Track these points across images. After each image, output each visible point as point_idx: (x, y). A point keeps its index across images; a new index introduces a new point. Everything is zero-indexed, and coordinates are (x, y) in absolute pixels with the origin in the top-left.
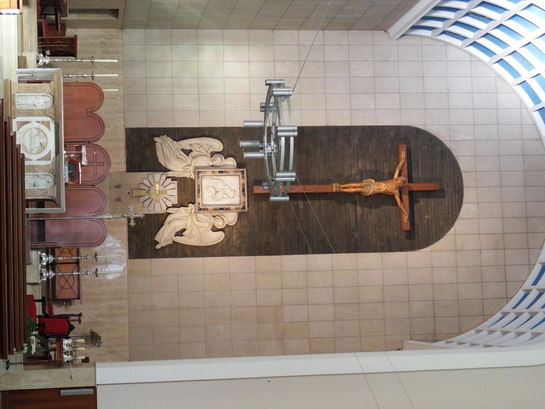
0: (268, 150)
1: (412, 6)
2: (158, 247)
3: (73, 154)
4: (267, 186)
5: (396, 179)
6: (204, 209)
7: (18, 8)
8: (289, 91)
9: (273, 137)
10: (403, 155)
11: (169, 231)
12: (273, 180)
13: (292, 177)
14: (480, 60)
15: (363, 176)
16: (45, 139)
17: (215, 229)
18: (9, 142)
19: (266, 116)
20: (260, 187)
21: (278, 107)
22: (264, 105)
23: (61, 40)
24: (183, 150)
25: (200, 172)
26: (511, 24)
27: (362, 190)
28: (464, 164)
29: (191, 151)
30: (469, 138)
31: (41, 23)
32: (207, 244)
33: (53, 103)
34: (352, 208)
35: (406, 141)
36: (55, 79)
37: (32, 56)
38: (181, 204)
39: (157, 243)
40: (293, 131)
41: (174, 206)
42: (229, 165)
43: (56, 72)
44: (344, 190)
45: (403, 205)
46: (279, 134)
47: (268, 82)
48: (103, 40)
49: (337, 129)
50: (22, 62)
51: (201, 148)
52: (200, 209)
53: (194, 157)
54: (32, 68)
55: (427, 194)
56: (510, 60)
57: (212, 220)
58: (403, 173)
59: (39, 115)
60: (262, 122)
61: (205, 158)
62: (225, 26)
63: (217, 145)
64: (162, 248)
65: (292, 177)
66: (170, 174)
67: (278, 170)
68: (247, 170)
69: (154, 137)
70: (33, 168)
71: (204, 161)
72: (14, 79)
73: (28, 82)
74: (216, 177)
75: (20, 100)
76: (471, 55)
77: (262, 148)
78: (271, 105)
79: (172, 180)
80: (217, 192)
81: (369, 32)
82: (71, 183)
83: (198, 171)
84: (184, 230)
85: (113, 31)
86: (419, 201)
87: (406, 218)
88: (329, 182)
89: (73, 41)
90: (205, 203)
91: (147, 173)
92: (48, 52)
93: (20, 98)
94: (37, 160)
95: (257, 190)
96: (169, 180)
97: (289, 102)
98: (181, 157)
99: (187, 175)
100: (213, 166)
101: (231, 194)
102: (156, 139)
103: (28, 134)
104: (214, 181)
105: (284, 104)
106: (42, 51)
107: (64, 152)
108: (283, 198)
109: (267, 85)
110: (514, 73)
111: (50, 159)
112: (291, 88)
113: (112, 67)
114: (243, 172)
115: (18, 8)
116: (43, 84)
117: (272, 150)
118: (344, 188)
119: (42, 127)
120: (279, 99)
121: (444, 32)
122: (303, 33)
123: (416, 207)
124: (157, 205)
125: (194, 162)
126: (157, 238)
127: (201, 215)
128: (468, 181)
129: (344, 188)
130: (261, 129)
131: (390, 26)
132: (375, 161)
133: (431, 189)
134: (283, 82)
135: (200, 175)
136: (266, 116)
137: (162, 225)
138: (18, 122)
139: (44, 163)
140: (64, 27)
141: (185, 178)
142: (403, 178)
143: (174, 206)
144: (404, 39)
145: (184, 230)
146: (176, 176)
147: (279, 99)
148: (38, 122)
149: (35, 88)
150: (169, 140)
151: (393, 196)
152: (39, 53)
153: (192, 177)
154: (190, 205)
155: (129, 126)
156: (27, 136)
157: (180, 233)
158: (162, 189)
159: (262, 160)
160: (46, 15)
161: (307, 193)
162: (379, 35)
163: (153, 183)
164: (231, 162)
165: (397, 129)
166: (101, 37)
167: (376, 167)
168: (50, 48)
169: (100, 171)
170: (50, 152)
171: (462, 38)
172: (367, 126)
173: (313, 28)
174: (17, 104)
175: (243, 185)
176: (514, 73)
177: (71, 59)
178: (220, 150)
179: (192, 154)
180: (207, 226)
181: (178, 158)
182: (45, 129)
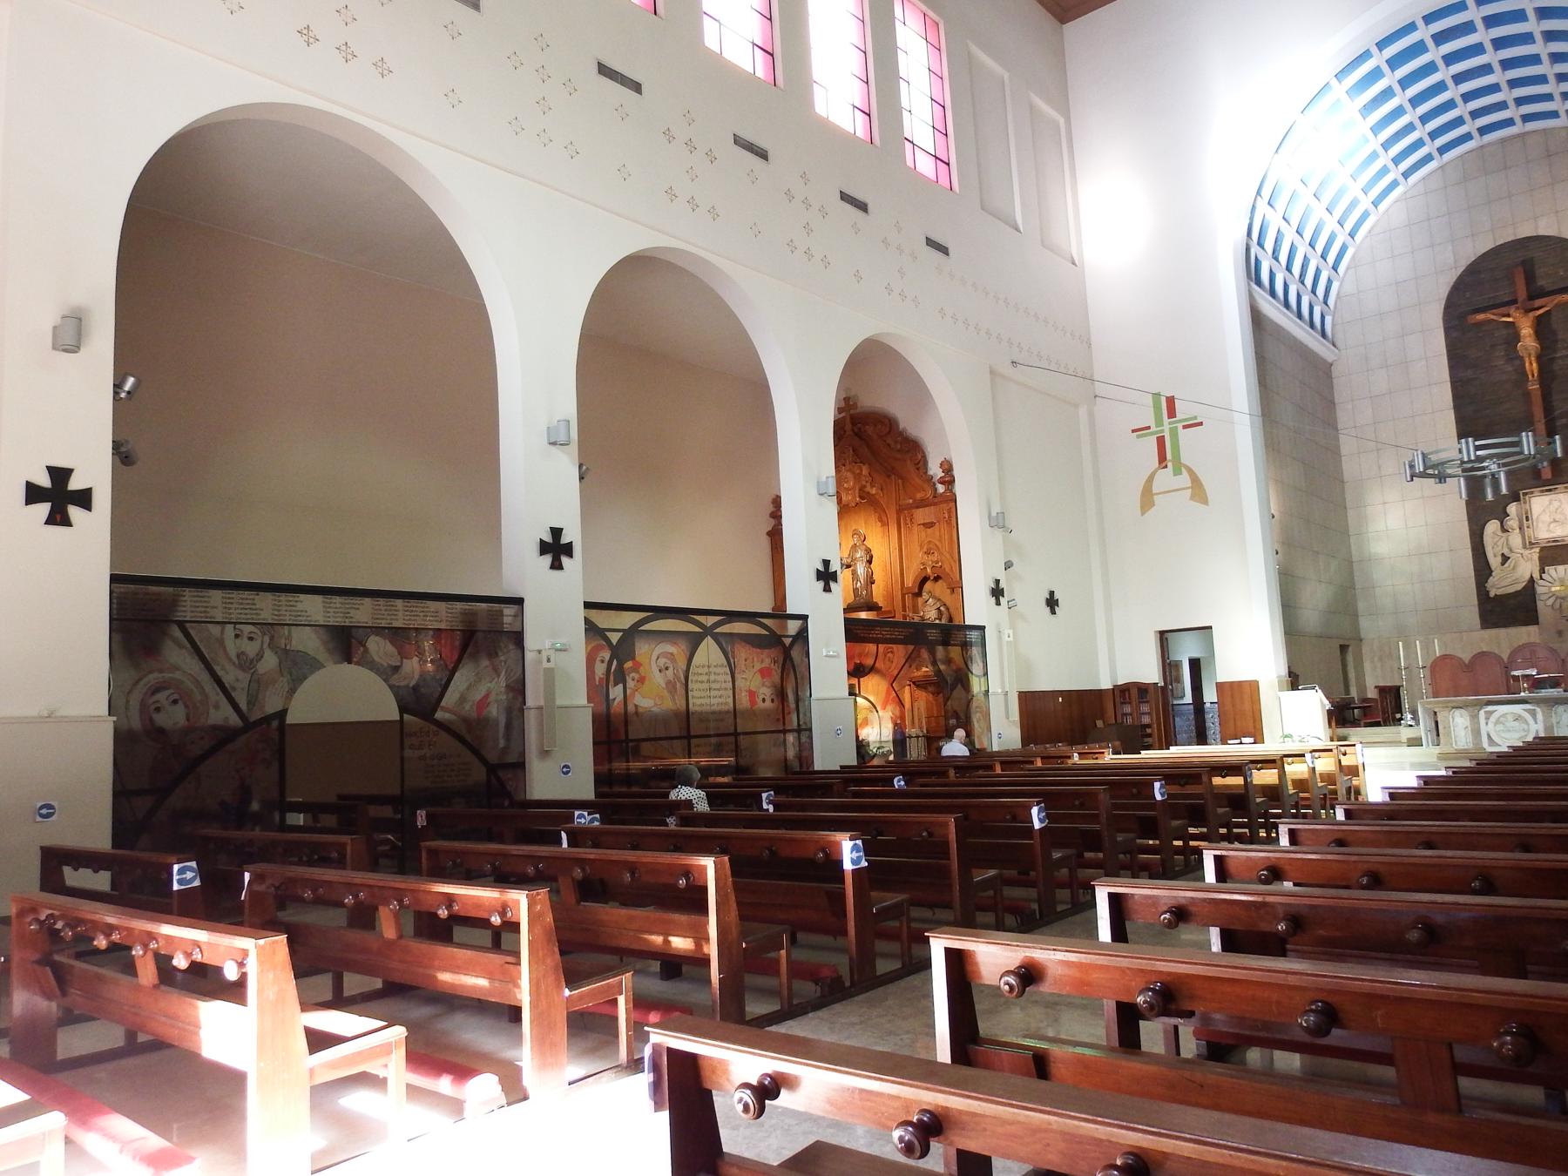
0: (1494, 468)
1: (1301, 343)
3: (61, 518)
4: (1542, 463)
5: (1514, 318)
7: (1354, 745)
8: (1417, 455)
9: (1477, 465)
10: (1481, 317)
12: (1534, 458)
13: (1528, 436)
14: (1353, 257)
15: (1514, 357)
18: (1522, 753)
19: (1450, 476)
20: (1543, 471)
21: (1438, 464)
22: (1437, 480)
23: (1382, 702)
24: (1503, 564)
25: (1530, 542)
26: (1308, 235)
29: (1503, 554)
31: (1365, 723)
32: (538, 894)
33: (1461, 708)
35: (1462, 317)
36: (1431, 706)
37: (1404, 732)
40: (1467, 443)
42: (1517, 510)
43: (1423, 706)
44: (1536, 375)
45: (1547, 304)
46: (1473, 458)
47: (1409, 479)
48: (1376, 659)
50: (1415, 742)
53: (1511, 550)
54: (1422, 731)
55: (1530, 278)
56: (1349, 226)
58: (1506, 312)
60: (1459, 480)
61: (1510, 538)
62: (1345, 533)
63: (1492, 527)
65: (1528, 436)
66: (1536, 575)
67: (1521, 453)
68: (1522, 490)
69: (1490, 598)
70: (1548, 728)
71: (1516, 539)
72: (1436, 750)
73: (1438, 735)
74: (1535, 523)
75: (1462, 744)
76: (1348, 269)
77: (1493, 475)
78: (1436, 472)
79: (1544, 573)
80: (1555, 521)
81: (1335, 381)
82: (1563, 685)
83: (1529, 544)
85: (1365, 650)
86: (1541, 286)
88: (1527, 395)
89: (1382, 690)
91: (1538, 603)
92: (1398, 716)
93: (1459, 743)
94: (1536, 723)
95: (1547, 474)
97: (1429, 454)
98: (1512, 565)
99: (1536, 557)
100: (1520, 529)
102: (1492, 594)
103: (1503, 735)
104: (1540, 525)
105: (1434, 458)
106: (1398, 722)
107: (1522, 694)
108: (1558, 443)
109: (1412, 480)
110: (1365, 216)
113: (1409, 647)
114: (1525, 494)
115: (1354, 745)
116: (1439, 720)
117: (1494, 463)
118: (1533, 376)
119: (1493, 719)
120: (1429, 464)
121: (1326, 303)
122: (1344, 450)
128: (1507, 236)
129: (1533, 376)
130: (1467, 479)
131: (1325, 361)
132: (1493, 346)
133: (1522, 276)
134: (1407, 462)
135: (1533, 542)
136: (1450, 476)
138: (1490, 745)
140: (1366, 700)
141: (1541, 559)
144: (1339, 344)
146: (1538, 568)
147: (1429, 464)
148: (1487, 724)
149: (1445, 728)
152: (1400, 725)
153: (1538, 550)
156: (1507, 735)
158: (1557, 583)
159: (1508, 474)
160: (1355, 719)
161: (1545, 417)
162: (1335, 372)
163: (1550, 595)
164: (1512, 509)
165: (1448, 330)
166: (1372, 662)
167: (1501, 345)
168: (1393, 714)
169: (1542, 653)
171: (1330, 282)
172: (1449, 363)
173: (1337, 439)
174: (1466, 747)
175: (1542, 491)
176: (1365, 216)
177: (1404, 693)
178: (1499, 523)
179: (1507, 553)
181: (1514, 569)
182: (1496, 715)
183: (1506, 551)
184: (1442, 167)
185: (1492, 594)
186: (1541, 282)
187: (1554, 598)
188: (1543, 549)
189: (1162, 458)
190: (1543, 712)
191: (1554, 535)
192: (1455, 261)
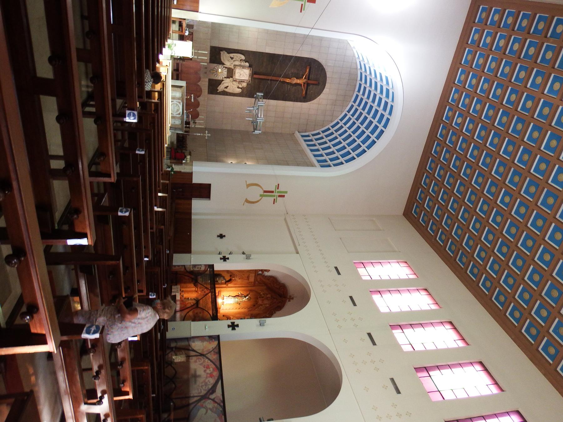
2: (218, 91)
6: (235, 81)
10: (308, 70)
11: (223, 86)
16: (179, 108)
17: (238, 88)
24: (230, 57)
27: (291, 82)
28: (328, 75)
29: (233, 58)
30: (332, 65)
34: (287, 86)
38: (228, 77)
39: (218, 90)
41: (225, 78)
49: (287, 56)
51: (237, 58)
52: (234, 81)
53: (234, 61)
57: (238, 84)
59: (177, 100)
61: (238, 62)
63: (243, 57)
64: (220, 92)
66: (225, 66)
71: (237, 63)
80: (241, 75)
84: (228, 87)
87: (304, 93)
90: (236, 78)
91: (216, 65)
96: (224, 68)
99: (231, 67)
101: (246, 76)
102: (221, 52)
104: (240, 71)
111: (180, 114)
112: (264, 102)
114: (251, 69)
119: (178, 103)
123: (309, 87)
124: (219, 77)
125: (234, 63)
126: (218, 88)
127: (234, 83)
132: (298, 70)
137: (220, 84)
139: (178, 116)
142: (305, 80)
143: (225, 78)
145: (228, 87)
148: (176, 102)
150: (226, 53)
151: (301, 85)
153: (233, 68)
154: (231, 78)
155: (212, 45)
157: (226, 87)
164: (247, 64)
165: (308, 59)
167: (298, 72)
170: (180, 112)
175: (250, 74)
180: (236, 86)
182: (179, 104)
183: (234, 59)
184: (357, 69)
185: (221, 52)
186: (311, 86)
187: (217, 69)
188: (233, 69)
189: (265, 192)
190: (179, 117)
191: (236, 73)
192: (328, 66)
